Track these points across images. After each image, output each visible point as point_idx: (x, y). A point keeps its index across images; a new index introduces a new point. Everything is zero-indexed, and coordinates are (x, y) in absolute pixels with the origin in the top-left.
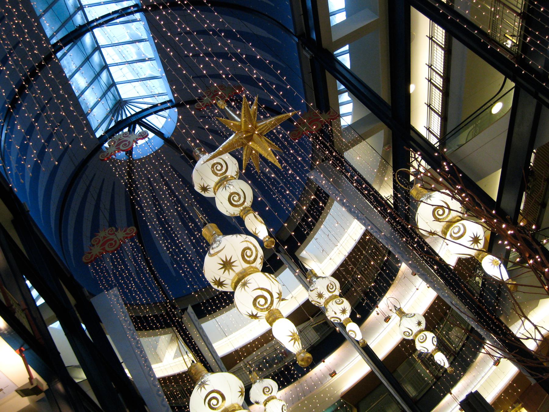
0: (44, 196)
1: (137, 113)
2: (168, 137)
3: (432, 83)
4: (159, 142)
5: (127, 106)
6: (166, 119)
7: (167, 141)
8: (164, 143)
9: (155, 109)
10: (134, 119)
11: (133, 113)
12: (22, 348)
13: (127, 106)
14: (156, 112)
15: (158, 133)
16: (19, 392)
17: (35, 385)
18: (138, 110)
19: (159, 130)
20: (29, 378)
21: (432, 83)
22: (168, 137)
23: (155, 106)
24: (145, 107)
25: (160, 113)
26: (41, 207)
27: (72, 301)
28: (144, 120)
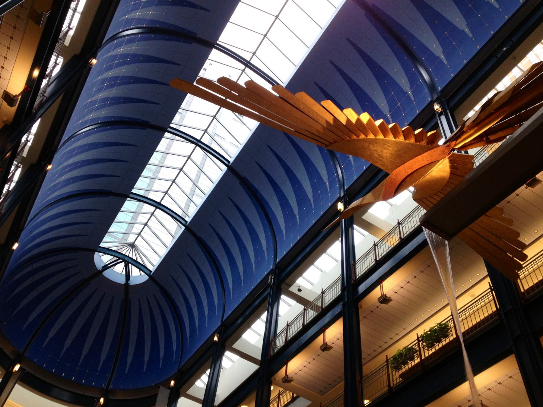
0: (38, 243)
1: (132, 259)
2: (129, 284)
3: (279, 396)
4: (122, 281)
5: (132, 249)
6: (140, 275)
7: (127, 284)
8: (124, 284)
9: (141, 267)
10: (126, 259)
11: (130, 256)
12: (29, 88)
13: (132, 249)
14: (140, 269)
15: (128, 276)
16: (5, 93)
17: (15, 99)
18: (134, 258)
19: (130, 275)
20: (16, 95)
21: (279, 396)
22: (129, 284)
23: (144, 266)
24: (140, 261)
25: (142, 263)
26: (35, 233)
27: (47, 152)
28: (130, 265)
